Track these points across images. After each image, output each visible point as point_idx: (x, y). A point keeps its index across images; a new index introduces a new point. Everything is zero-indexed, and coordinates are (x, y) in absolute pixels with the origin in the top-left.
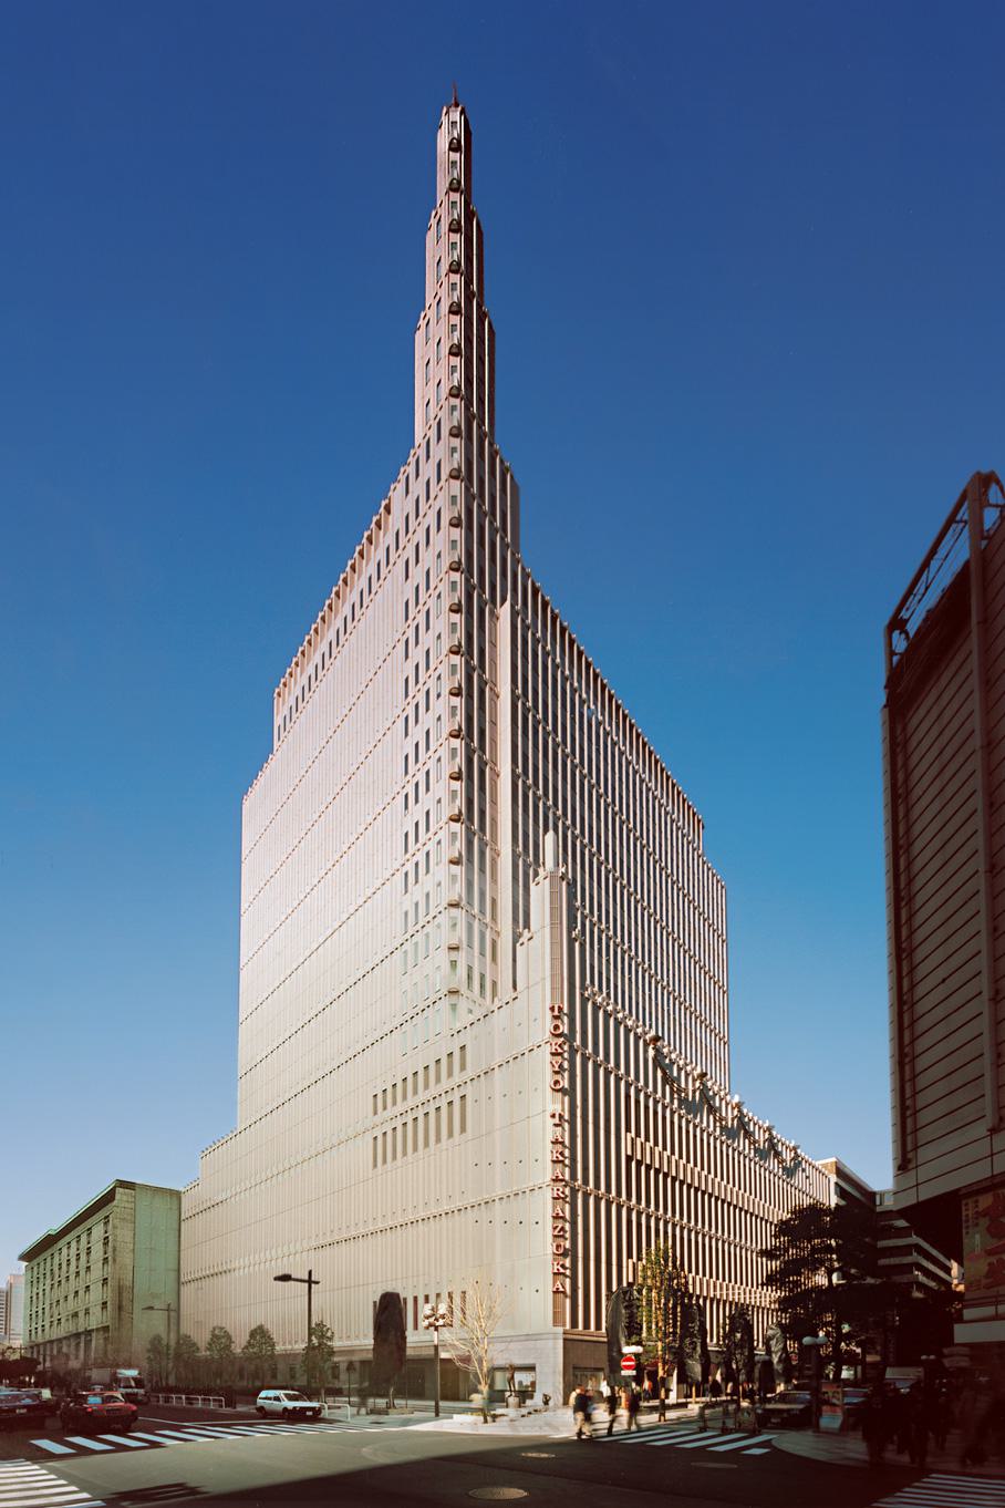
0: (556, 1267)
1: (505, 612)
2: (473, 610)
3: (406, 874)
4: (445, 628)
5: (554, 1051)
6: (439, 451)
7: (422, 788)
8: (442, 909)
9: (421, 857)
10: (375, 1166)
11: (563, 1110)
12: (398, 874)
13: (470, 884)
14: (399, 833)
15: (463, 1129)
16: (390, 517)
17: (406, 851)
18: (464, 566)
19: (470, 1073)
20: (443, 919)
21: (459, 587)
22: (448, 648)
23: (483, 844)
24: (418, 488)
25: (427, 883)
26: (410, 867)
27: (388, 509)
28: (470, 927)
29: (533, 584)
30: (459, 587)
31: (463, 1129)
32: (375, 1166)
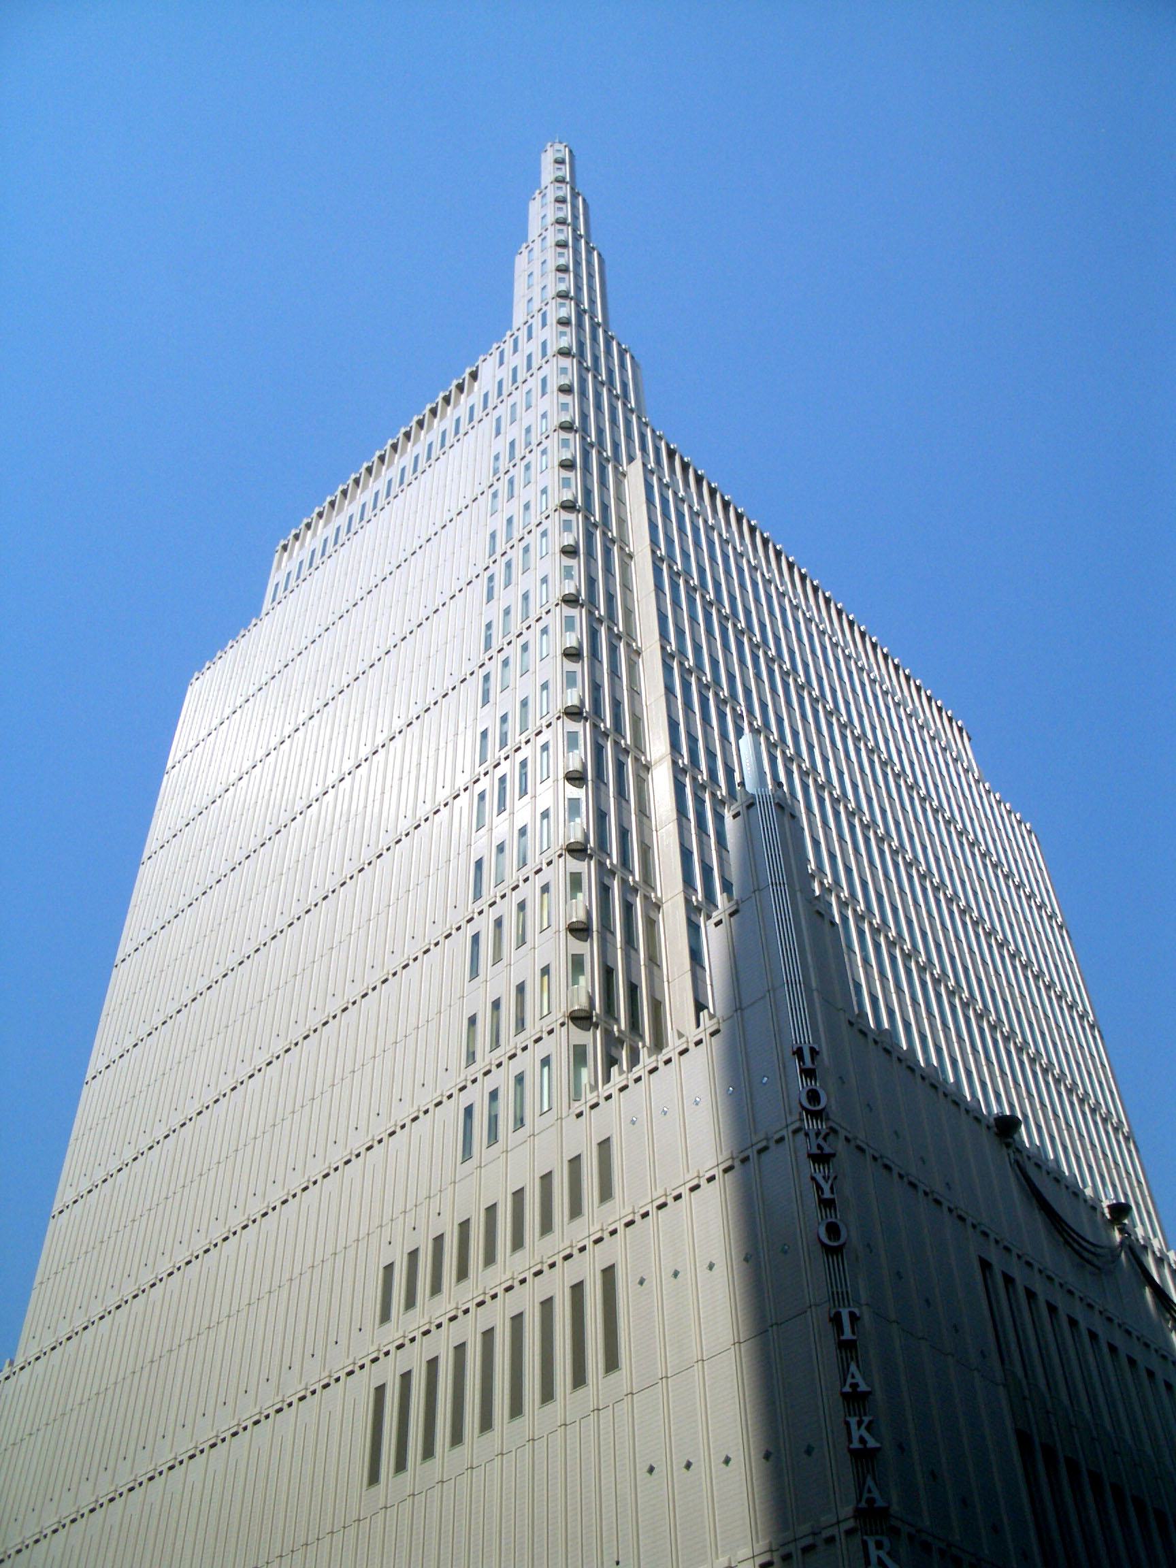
0: (855, 1435)
1: (635, 472)
2: (591, 458)
3: (469, 1111)
4: (546, 483)
5: (815, 1151)
6: (540, 335)
7: (513, 787)
8: (556, 1026)
9: (507, 907)
10: (374, 1478)
11: (817, 1038)
12: (465, 796)
13: (601, 816)
14: (469, 732)
15: (612, 1363)
16: (476, 384)
17: (478, 895)
18: (587, 708)
19: (619, 1210)
20: (558, 875)
21: (581, 742)
22: (557, 502)
23: (614, 638)
24: (513, 360)
25: (523, 812)
26: (485, 926)
27: (474, 376)
28: (605, 891)
29: (668, 446)
30: (581, 742)
31: (612, 1363)
32: (374, 1478)
